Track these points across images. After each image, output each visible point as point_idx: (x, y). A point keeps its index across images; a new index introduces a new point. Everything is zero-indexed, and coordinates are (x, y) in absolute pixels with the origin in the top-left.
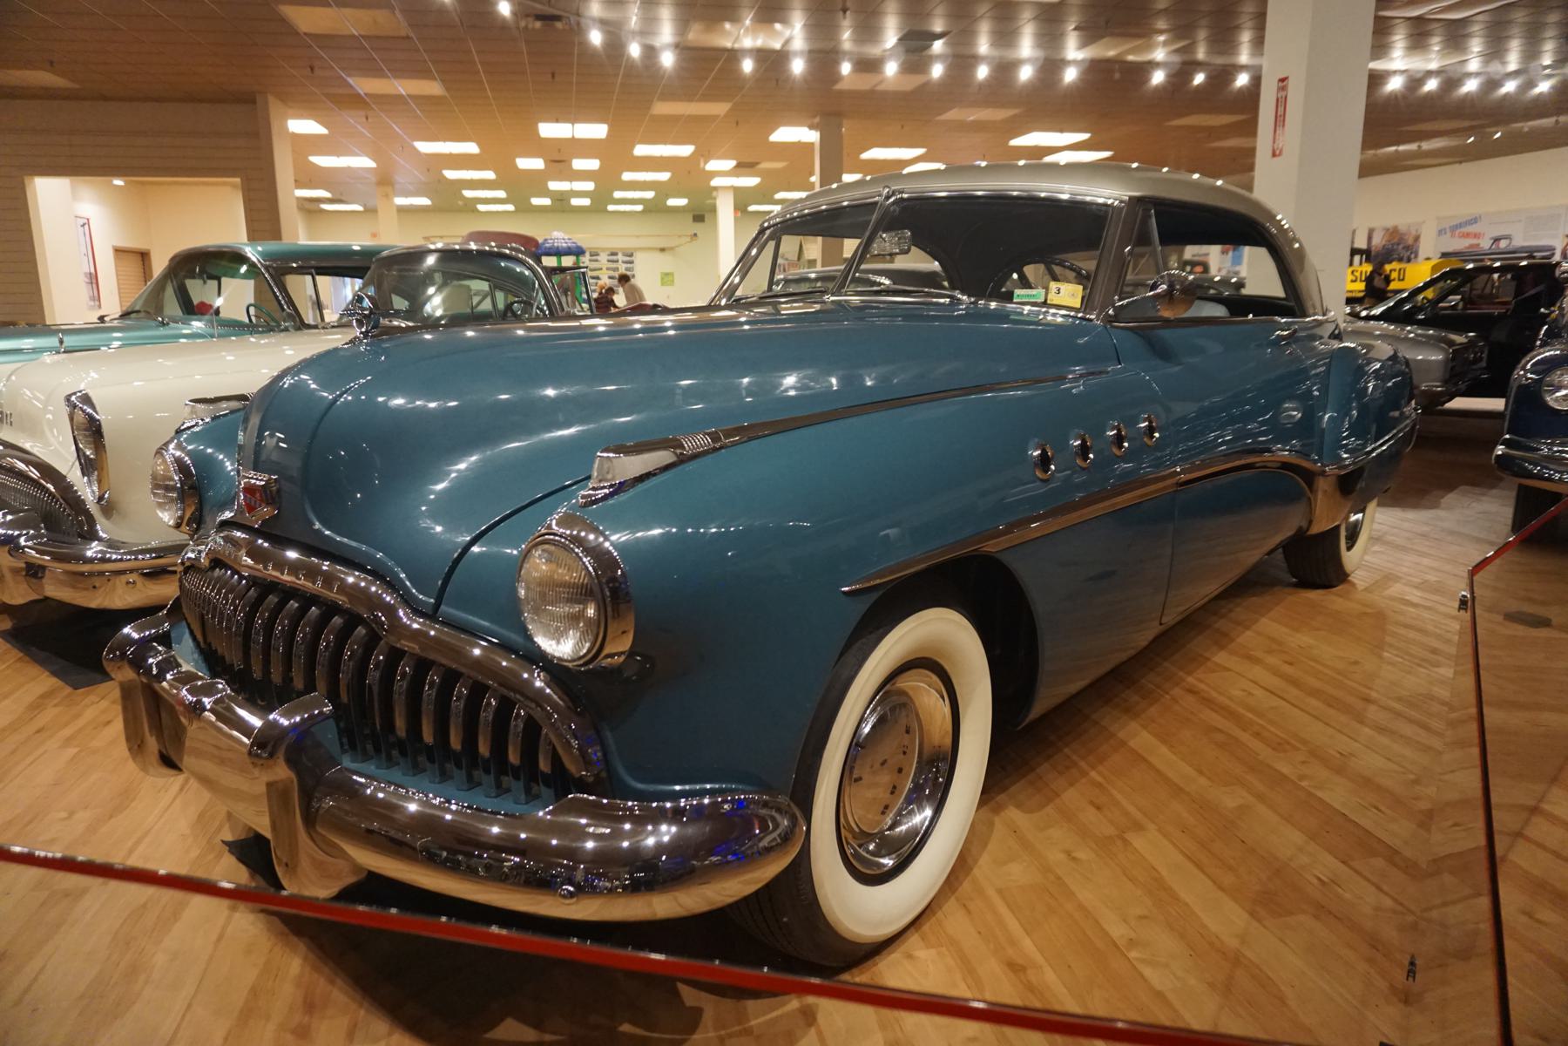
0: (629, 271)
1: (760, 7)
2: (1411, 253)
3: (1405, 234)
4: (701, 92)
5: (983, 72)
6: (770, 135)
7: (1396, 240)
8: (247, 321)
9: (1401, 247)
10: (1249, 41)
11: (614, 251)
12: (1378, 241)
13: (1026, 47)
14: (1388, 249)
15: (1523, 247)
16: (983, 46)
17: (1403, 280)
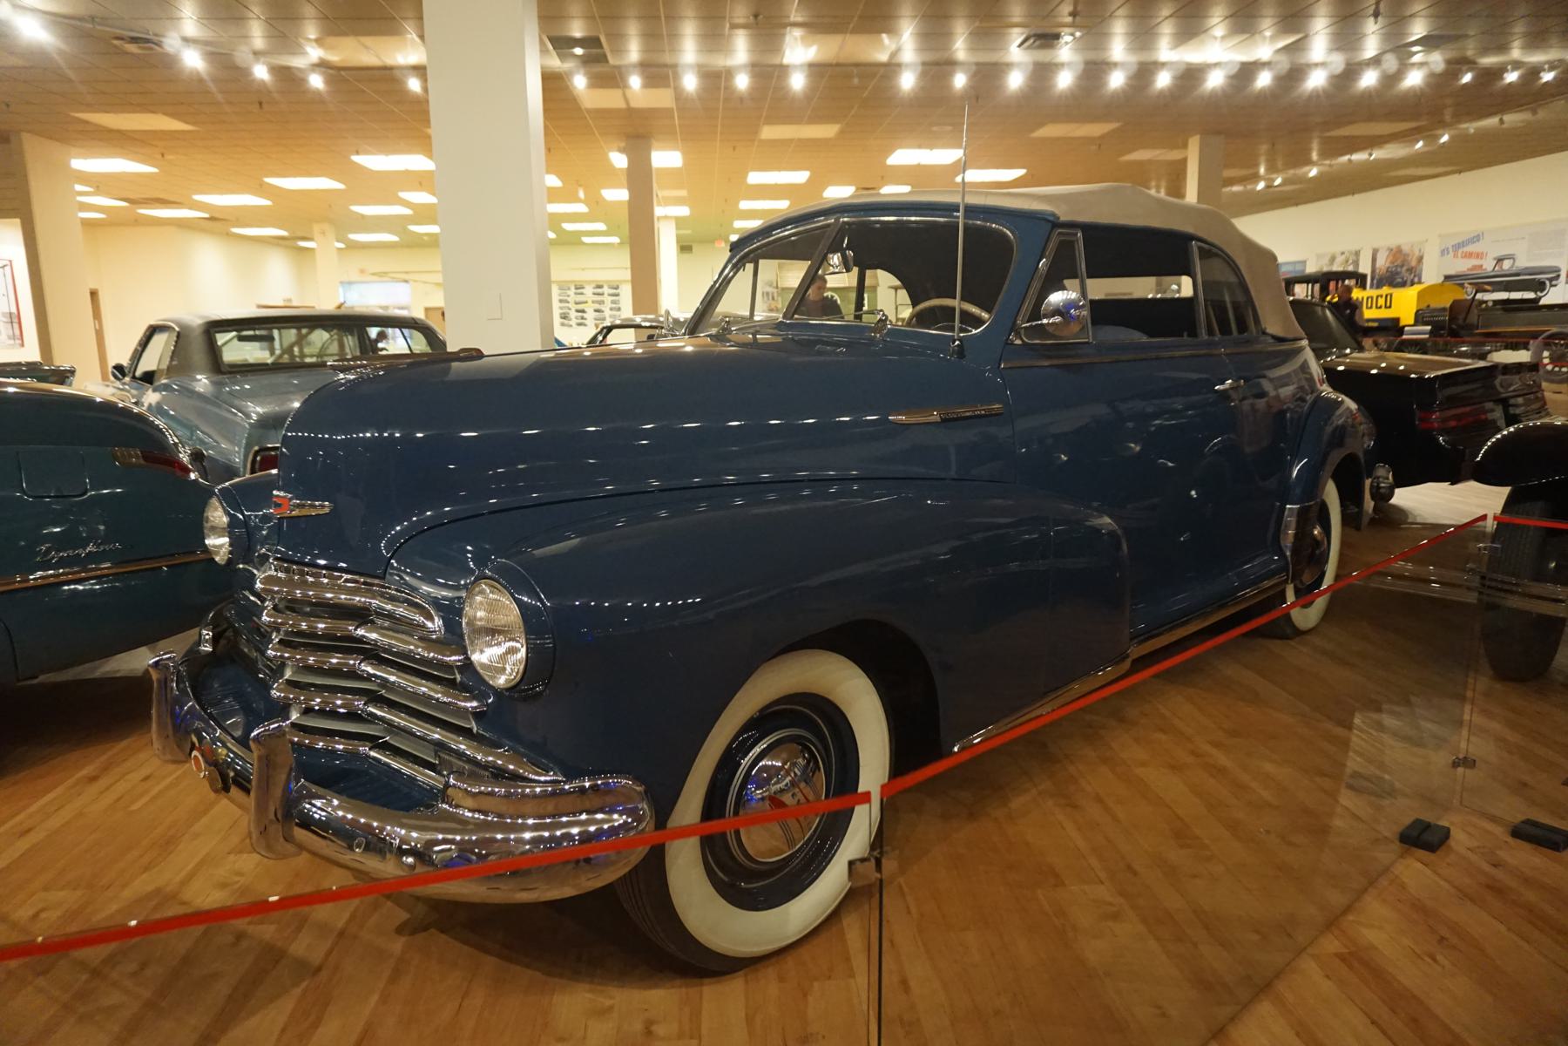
0: (615, 303)
1: (923, 16)
2: (1415, 276)
3: (1408, 255)
4: (764, 114)
5: (960, 81)
6: (887, 158)
7: (1399, 262)
8: (409, 352)
9: (1404, 268)
10: (1170, 34)
11: (601, 284)
12: (1382, 262)
13: (1118, 48)
14: (1391, 272)
15: (1527, 268)
16: (960, 48)
17: (1390, 307)
